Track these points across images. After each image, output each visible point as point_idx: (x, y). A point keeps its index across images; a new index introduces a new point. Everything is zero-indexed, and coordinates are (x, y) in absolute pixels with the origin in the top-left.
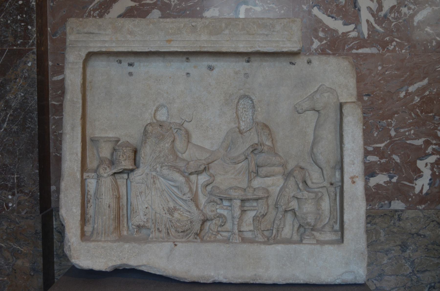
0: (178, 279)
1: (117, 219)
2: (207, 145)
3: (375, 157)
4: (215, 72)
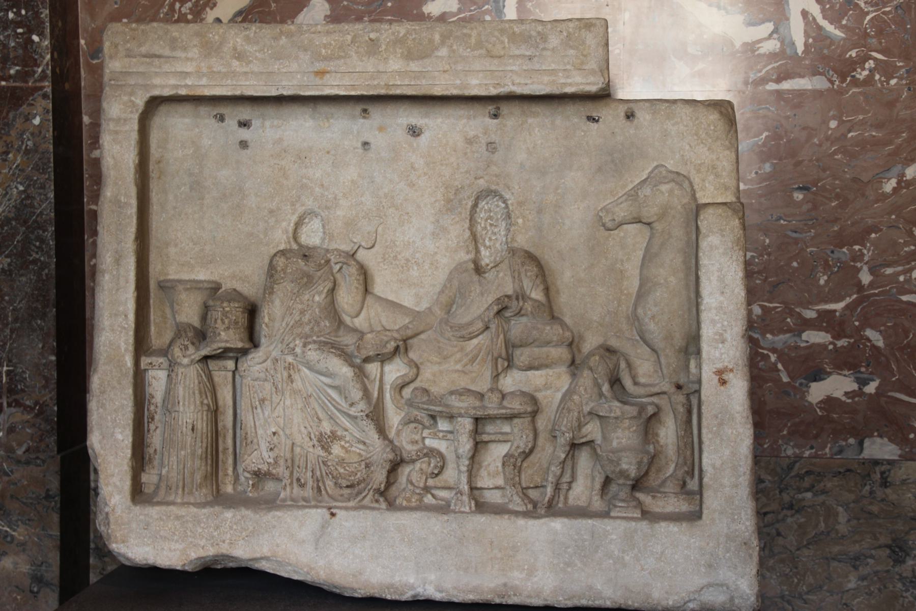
0: (338, 591)
1: (209, 457)
2: (407, 300)
3: (822, 334)
4: (424, 139)
